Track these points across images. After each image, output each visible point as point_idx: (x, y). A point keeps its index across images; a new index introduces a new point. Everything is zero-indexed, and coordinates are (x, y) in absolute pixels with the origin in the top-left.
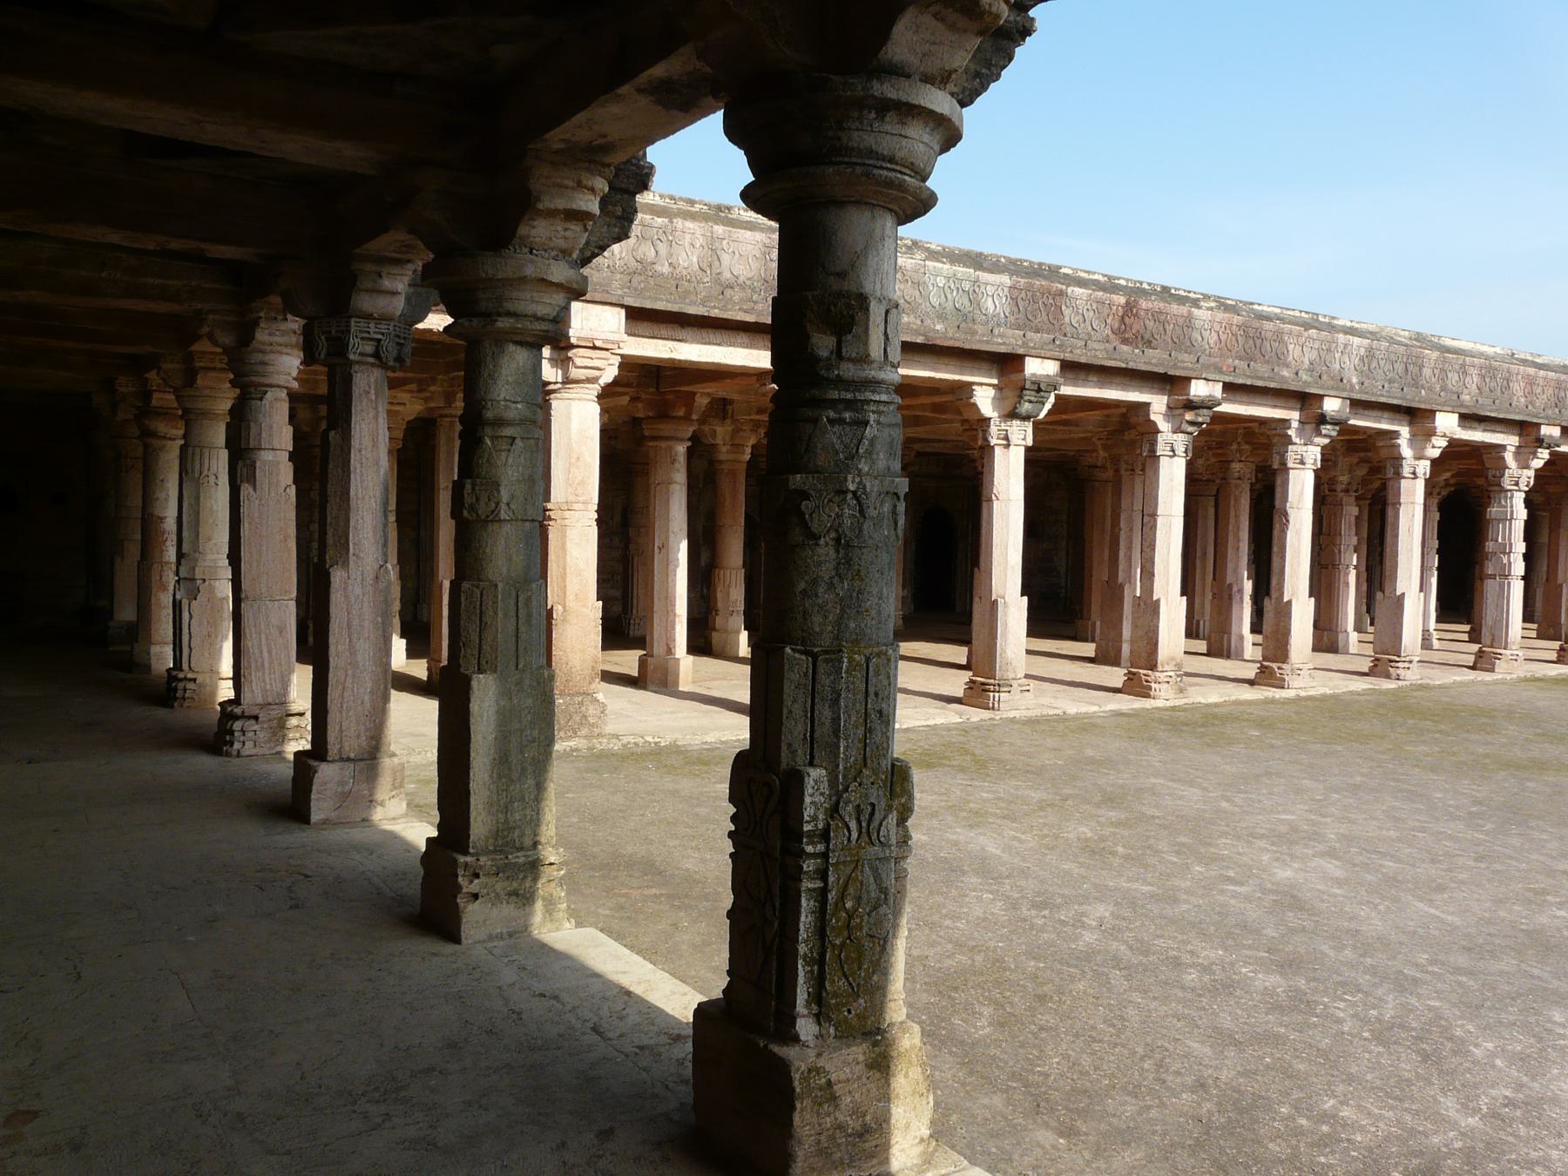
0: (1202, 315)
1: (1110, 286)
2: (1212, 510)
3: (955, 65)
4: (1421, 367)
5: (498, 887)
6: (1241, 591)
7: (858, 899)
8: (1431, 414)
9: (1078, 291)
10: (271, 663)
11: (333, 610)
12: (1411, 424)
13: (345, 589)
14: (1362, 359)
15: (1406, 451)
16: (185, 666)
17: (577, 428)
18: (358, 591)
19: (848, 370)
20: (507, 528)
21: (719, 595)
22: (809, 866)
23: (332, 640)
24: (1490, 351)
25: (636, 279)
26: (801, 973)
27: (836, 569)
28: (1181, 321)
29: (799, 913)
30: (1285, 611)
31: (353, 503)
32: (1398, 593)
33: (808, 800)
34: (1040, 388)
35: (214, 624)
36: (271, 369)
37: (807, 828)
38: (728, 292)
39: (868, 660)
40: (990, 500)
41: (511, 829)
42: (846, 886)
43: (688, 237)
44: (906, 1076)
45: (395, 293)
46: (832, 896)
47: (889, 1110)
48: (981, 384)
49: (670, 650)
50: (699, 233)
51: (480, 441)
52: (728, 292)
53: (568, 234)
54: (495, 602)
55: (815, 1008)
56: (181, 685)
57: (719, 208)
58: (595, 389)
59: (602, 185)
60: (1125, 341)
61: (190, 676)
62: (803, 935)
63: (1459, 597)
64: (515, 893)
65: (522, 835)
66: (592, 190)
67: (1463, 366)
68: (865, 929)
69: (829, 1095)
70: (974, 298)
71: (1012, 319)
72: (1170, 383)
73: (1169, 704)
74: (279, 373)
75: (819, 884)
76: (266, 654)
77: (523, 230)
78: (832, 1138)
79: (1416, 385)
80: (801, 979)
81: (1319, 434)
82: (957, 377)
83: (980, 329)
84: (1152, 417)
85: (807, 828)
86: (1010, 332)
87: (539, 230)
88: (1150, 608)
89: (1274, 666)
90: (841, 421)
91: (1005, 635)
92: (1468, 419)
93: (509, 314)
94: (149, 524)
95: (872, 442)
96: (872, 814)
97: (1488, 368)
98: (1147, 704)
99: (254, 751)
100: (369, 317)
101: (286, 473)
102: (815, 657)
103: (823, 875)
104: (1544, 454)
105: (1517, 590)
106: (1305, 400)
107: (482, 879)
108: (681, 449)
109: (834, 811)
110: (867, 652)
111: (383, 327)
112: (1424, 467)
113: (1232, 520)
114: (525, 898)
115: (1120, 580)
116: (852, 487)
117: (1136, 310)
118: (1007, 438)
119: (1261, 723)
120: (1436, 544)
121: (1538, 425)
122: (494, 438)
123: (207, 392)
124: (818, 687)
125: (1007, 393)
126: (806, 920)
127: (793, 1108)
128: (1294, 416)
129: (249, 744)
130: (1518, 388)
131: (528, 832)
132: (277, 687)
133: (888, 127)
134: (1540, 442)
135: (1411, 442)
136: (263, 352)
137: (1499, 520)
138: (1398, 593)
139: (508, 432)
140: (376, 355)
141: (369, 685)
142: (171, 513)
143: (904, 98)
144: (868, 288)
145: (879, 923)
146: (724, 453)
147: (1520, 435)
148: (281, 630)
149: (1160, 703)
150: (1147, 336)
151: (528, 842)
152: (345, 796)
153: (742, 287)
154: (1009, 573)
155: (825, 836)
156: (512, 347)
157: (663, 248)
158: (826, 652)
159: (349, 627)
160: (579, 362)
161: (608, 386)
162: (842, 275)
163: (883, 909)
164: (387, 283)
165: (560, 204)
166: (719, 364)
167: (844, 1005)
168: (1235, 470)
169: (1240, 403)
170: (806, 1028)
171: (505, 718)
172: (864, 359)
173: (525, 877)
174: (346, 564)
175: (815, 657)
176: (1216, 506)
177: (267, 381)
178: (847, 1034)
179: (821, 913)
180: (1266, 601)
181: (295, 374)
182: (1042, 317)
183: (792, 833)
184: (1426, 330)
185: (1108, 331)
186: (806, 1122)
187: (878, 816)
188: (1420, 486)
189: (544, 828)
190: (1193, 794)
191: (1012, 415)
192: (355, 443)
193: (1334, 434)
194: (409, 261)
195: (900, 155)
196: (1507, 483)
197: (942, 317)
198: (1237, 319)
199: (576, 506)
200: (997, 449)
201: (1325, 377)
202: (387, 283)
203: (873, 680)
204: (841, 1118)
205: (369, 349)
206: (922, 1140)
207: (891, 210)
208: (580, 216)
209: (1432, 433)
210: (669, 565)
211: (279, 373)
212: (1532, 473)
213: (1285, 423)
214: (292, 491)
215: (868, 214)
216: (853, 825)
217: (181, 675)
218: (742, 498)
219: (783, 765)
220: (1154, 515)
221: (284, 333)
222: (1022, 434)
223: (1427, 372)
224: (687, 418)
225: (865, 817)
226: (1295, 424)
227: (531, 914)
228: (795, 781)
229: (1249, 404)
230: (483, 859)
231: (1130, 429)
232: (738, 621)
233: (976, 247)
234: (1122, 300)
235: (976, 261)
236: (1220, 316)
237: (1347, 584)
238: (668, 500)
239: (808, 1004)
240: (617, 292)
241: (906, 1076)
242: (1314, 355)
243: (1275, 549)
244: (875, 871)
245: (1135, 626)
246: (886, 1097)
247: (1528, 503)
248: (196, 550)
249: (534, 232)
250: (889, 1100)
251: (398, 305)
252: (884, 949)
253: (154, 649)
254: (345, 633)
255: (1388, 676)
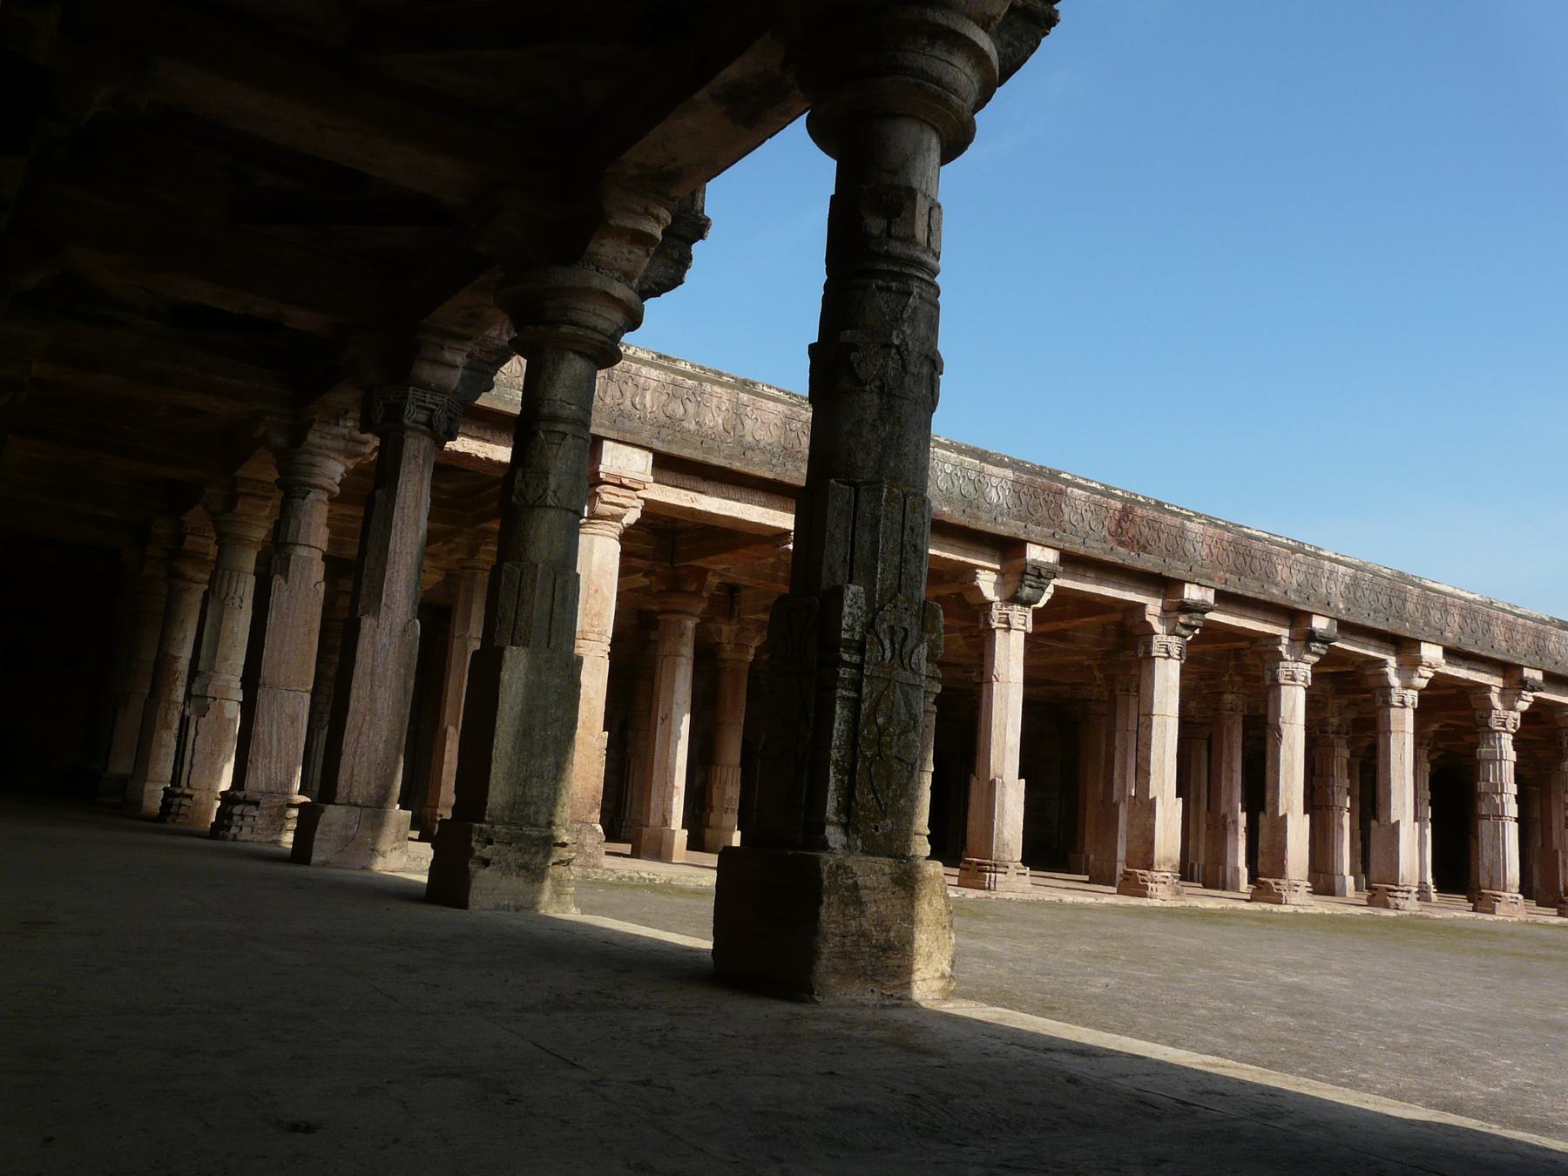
0: (1194, 527)
1: (1107, 493)
2: (1204, 753)
3: (995, 11)
4: (1405, 601)
5: (510, 856)
6: (1235, 822)
7: (889, 719)
8: (1416, 643)
9: (1077, 492)
10: (279, 751)
11: (359, 656)
12: (1397, 654)
13: (373, 637)
14: (1347, 587)
15: (1394, 681)
16: (184, 783)
17: (599, 558)
18: (385, 640)
19: (896, 248)
20: (551, 514)
21: (715, 792)
22: (844, 673)
23: (354, 684)
24: (1471, 597)
25: (664, 432)
26: (832, 780)
27: (880, 413)
28: (1174, 531)
29: (833, 719)
30: (1280, 825)
31: (391, 557)
32: (1393, 821)
33: (846, 610)
34: (1041, 574)
35: (218, 744)
36: (317, 470)
37: (845, 635)
38: (749, 454)
39: (905, 497)
40: (991, 682)
41: (527, 804)
42: (877, 704)
43: (715, 400)
44: (930, 904)
45: (454, 366)
46: (865, 706)
47: (912, 934)
48: (984, 568)
49: (666, 822)
50: (725, 397)
51: (535, 434)
52: (749, 454)
53: (632, 256)
54: (534, 581)
55: (844, 819)
56: (177, 800)
57: (745, 382)
58: (615, 529)
59: (665, 215)
60: (1121, 543)
61: (187, 791)
62: (836, 742)
63: (1457, 869)
64: (524, 867)
65: (537, 813)
66: (657, 219)
67: (1445, 604)
68: (894, 751)
69: (854, 898)
70: (979, 485)
71: (1014, 510)
72: (1165, 585)
73: (1165, 904)
74: (324, 476)
75: (852, 694)
76: (275, 742)
77: (592, 247)
78: (856, 944)
79: (1400, 617)
80: (832, 787)
81: (1309, 652)
82: (961, 558)
83: (984, 516)
84: (1148, 618)
85: (845, 635)
86: (1013, 522)
87: (608, 249)
88: (1147, 807)
89: (1271, 881)
90: (888, 289)
91: (1002, 815)
92: (1452, 654)
93: (571, 323)
94: (163, 663)
95: (915, 310)
96: (905, 639)
97: (1470, 611)
98: (1144, 902)
99: (250, 837)
100: (426, 387)
101: (318, 571)
102: (857, 488)
103: (857, 687)
104: (1529, 697)
105: (1512, 832)
106: (1295, 617)
107: (495, 845)
108: (690, 624)
109: (870, 627)
110: (906, 489)
111: (438, 399)
112: (1412, 697)
113: (1225, 752)
114: (536, 875)
115: (1115, 798)
116: (896, 342)
117: (1128, 517)
118: (1007, 622)
119: (1256, 919)
120: (1428, 795)
121: (1521, 667)
122: (548, 432)
123: (244, 518)
124: (859, 513)
125: (1009, 578)
126: (839, 727)
127: (820, 902)
128: (1284, 633)
129: (246, 830)
130: (1498, 631)
131: (544, 810)
132: (281, 777)
133: (936, 53)
134: (1524, 684)
135: (1400, 669)
136: (311, 453)
137: (1489, 761)
138: (1393, 821)
139: (561, 427)
140: (429, 424)
141: (385, 734)
142: (186, 653)
143: (952, 26)
144: (915, 185)
145: (908, 747)
146: (728, 651)
147: (1504, 677)
148: (294, 720)
149: (1157, 903)
150: (1142, 541)
151: (542, 820)
152: (347, 841)
153: (763, 450)
154: (1008, 753)
155: (861, 650)
156: (571, 356)
157: (691, 407)
158: (867, 483)
159: (373, 674)
160: (605, 497)
161: (630, 527)
162: (894, 172)
163: (912, 735)
164: (448, 356)
165: (630, 224)
166: (736, 519)
167: (872, 820)
168: (1229, 683)
169: (1232, 614)
170: (834, 836)
171: (533, 692)
172: (910, 239)
173: (537, 853)
174: (376, 614)
175: (857, 488)
176: (1209, 753)
177: (313, 481)
178: (872, 850)
179: (854, 723)
180: (1262, 817)
181: (338, 480)
182: (1042, 512)
183: (829, 644)
184: (1408, 570)
185: (1105, 533)
186: (829, 914)
187: (910, 643)
188: (1409, 715)
189: (559, 808)
190: (1195, 942)
191: (1013, 599)
192: (399, 501)
193: (1323, 652)
194: (470, 339)
195: (947, 79)
196: (1494, 724)
197: (948, 500)
198: (1226, 535)
199: (590, 636)
200: (998, 633)
201: (1312, 599)
202: (448, 356)
203: (909, 515)
204: (866, 925)
205: (422, 417)
206: (943, 976)
207: (937, 130)
208: (642, 239)
209: (1417, 662)
210: (671, 737)
211: (324, 476)
212: (1518, 715)
213: (1276, 638)
214: (322, 588)
215: (916, 127)
216: (887, 643)
217: (178, 791)
218: (743, 696)
219: (824, 586)
220: (1150, 715)
221: (335, 437)
222: (1022, 619)
223: (1410, 606)
224: (698, 593)
225: (898, 639)
226: (1285, 641)
227: (540, 891)
228: (837, 594)
229: (1240, 616)
230: (497, 828)
231: (1128, 635)
232: (733, 819)
233: (983, 446)
234: (1119, 505)
235: (984, 456)
236: (1211, 531)
237: (1342, 827)
238: (674, 673)
239: (838, 812)
240: (644, 438)
241: (930, 904)
242: (1301, 578)
243: (1269, 764)
244: (905, 695)
245: (1130, 825)
246: (910, 918)
247: (1517, 745)
248: (212, 668)
249: (602, 250)
250: (912, 922)
251: (454, 378)
252: (911, 773)
253: (149, 787)
254: (368, 678)
255: (1387, 906)
